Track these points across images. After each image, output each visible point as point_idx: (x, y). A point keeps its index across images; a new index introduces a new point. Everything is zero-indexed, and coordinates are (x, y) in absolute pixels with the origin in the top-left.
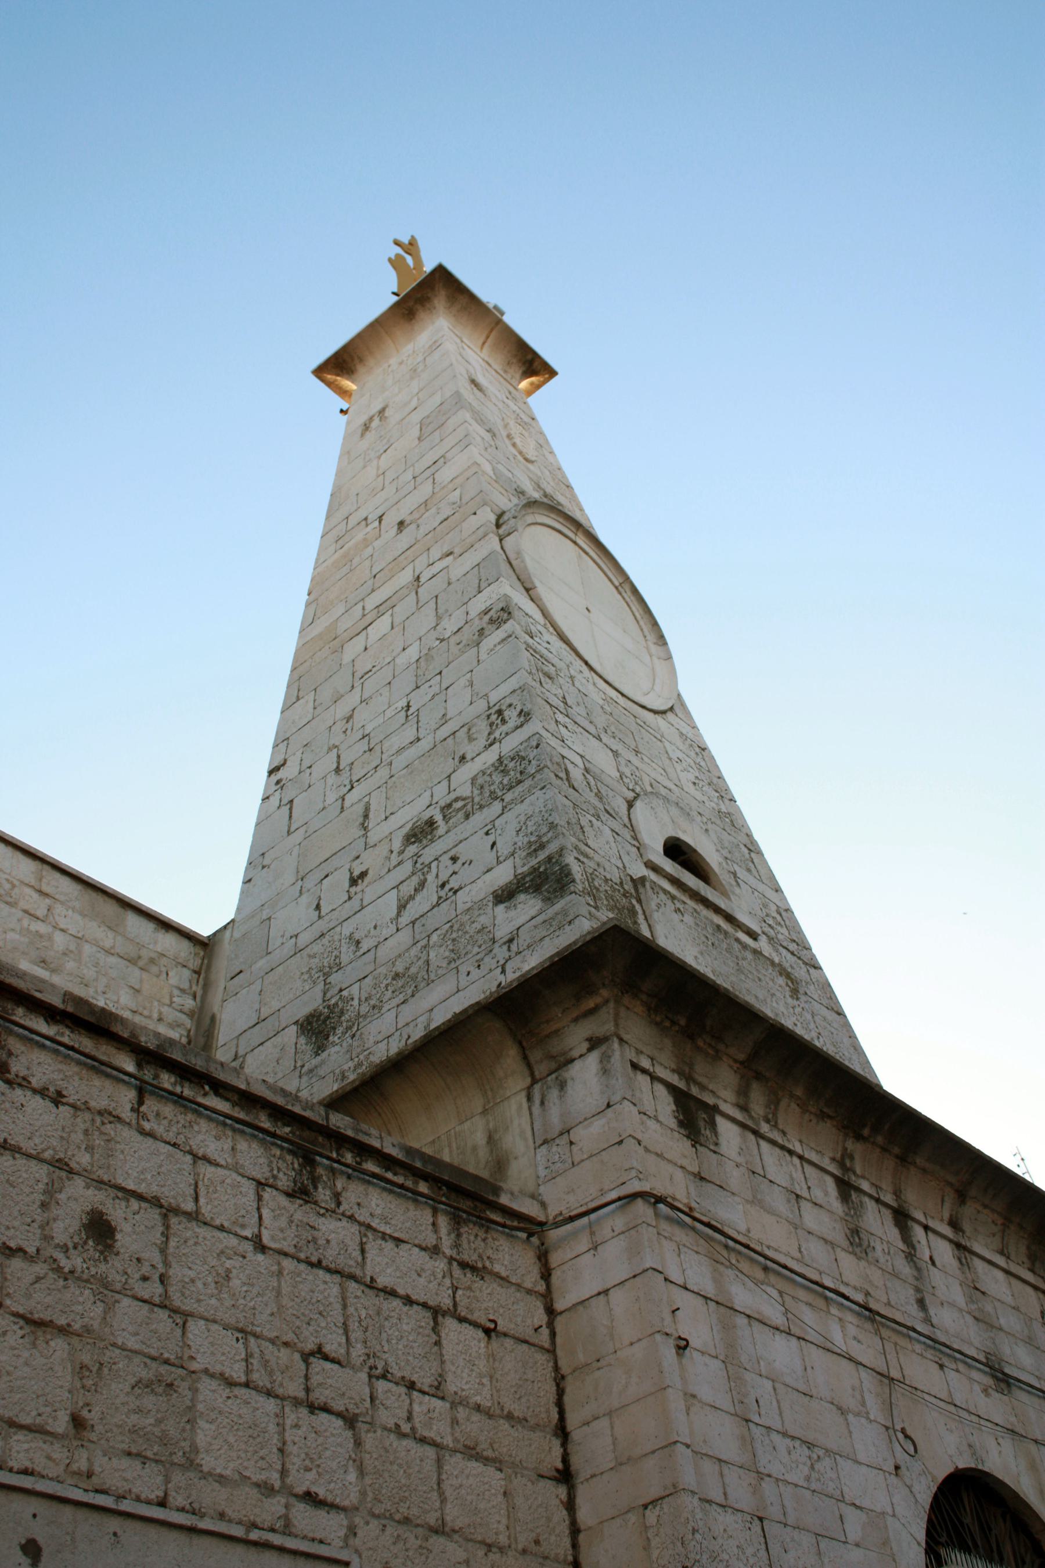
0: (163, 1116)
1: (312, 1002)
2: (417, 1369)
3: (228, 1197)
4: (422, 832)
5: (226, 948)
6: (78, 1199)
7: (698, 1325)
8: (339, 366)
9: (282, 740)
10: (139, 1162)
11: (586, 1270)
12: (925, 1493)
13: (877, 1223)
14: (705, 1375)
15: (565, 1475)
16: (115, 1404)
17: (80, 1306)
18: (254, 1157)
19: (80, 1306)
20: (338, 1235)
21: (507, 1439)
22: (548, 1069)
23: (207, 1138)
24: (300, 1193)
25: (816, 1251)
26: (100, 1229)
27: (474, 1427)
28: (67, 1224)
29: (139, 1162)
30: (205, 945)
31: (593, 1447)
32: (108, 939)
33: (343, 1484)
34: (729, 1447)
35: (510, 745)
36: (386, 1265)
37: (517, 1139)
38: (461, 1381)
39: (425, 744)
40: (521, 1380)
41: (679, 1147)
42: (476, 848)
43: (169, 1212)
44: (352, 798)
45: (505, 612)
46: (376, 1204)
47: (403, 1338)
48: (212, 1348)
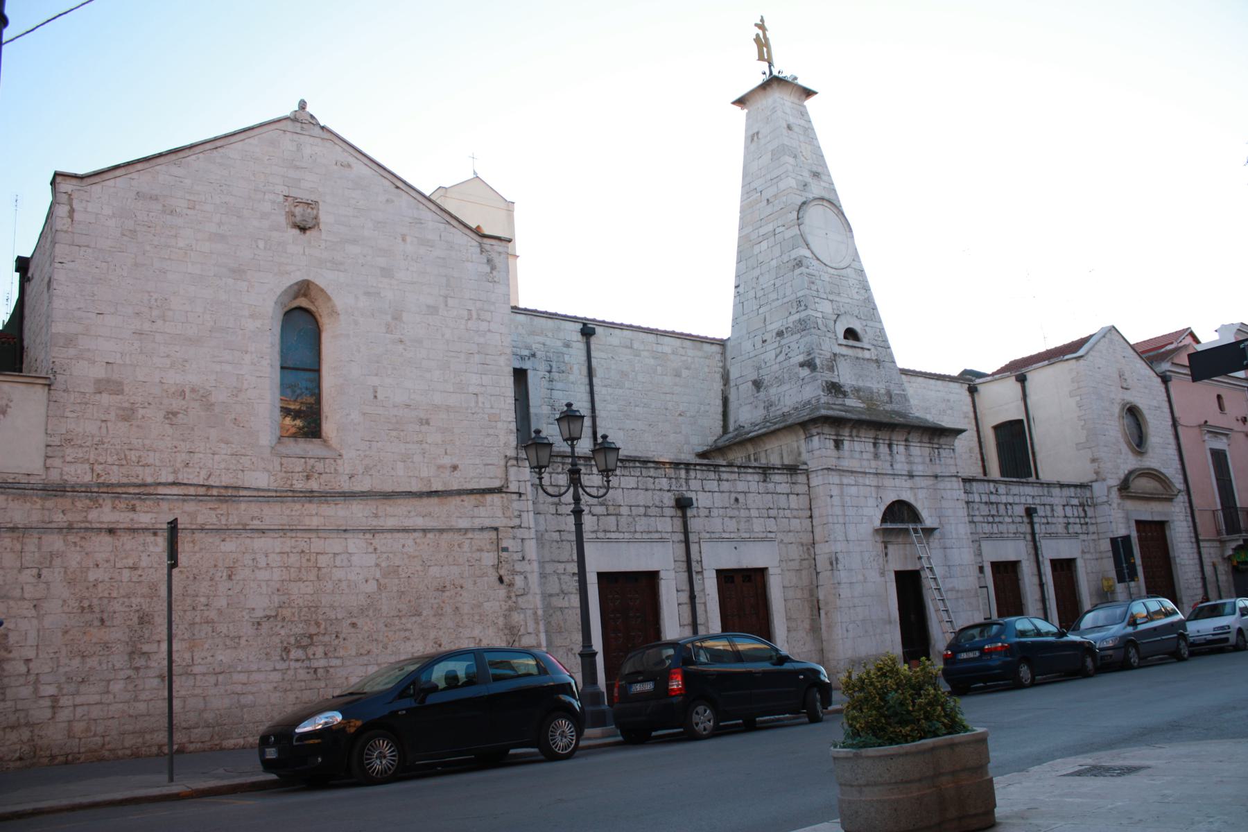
0: (743, 476)
1: (755, 377)
2: (778, 283)
3: (754, 487)
4: (780, 334)
5: (729, 343)
6: (733, 496)
7: (835, 491)
8: (741, 102)
9: (738, 276)
10: (741, 486)
11: (816, 480)
12: (883, 508)
13: (883, 449)
14: (836, 500)
15: (811, 517)
16: (743, 526)
17: (736, 513)
18: (756, 477)
19: (736, 513)
20: (771, 486)
21: (801, 513)
22: (809, 437)
23: (749, 477)
24: (765, 481)
25: (865, 463)
26: (737, 500)
27: (795, 513)
28: (732, 501)
29: (741, 486)
30: (722, 343)
31: (816, 513)
32: (699, 354)
33: (774, 528)
34: (840, 513)
35: (803, 315)
36: (780, 489)
37: (803, 449)
38: (793, 505)
39: (780, 302)
40: (804, 501)
41: (834, 453)
42: (794, 346)
43: (745, 493)
44: (761, 311)
45: (799, 264)
46: (777, 478)
47: (782, 501)
48: (754, 513)
